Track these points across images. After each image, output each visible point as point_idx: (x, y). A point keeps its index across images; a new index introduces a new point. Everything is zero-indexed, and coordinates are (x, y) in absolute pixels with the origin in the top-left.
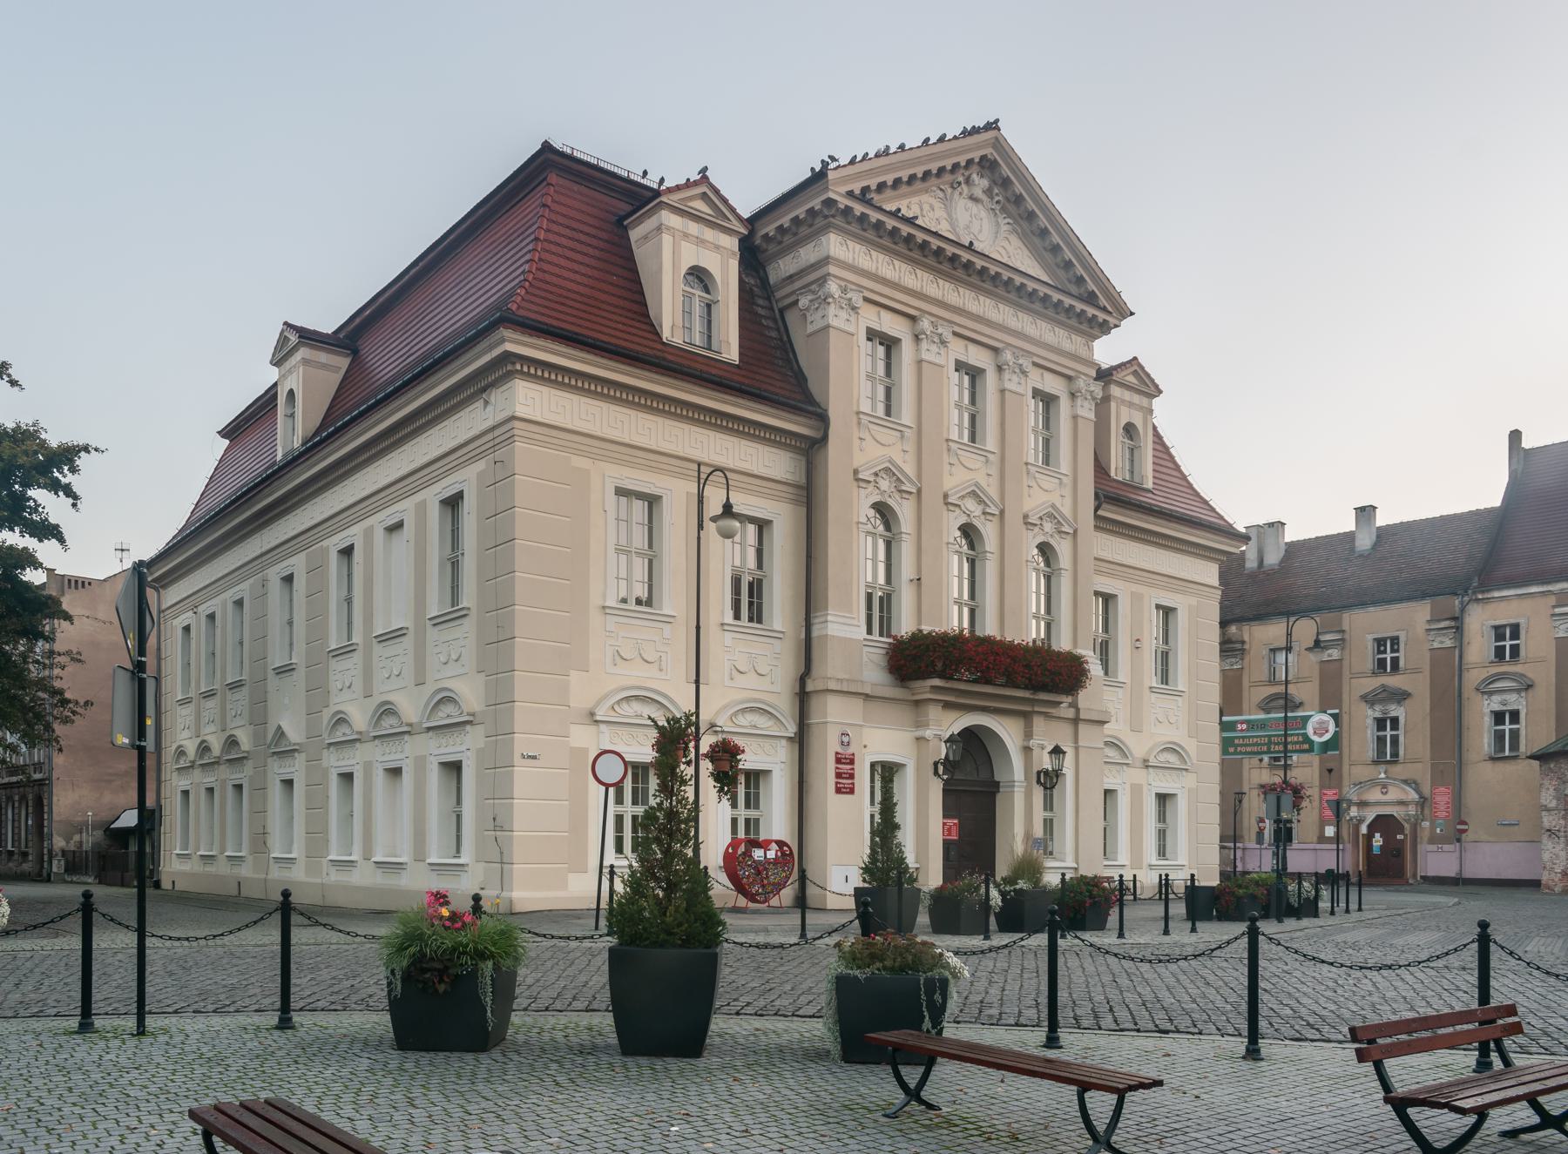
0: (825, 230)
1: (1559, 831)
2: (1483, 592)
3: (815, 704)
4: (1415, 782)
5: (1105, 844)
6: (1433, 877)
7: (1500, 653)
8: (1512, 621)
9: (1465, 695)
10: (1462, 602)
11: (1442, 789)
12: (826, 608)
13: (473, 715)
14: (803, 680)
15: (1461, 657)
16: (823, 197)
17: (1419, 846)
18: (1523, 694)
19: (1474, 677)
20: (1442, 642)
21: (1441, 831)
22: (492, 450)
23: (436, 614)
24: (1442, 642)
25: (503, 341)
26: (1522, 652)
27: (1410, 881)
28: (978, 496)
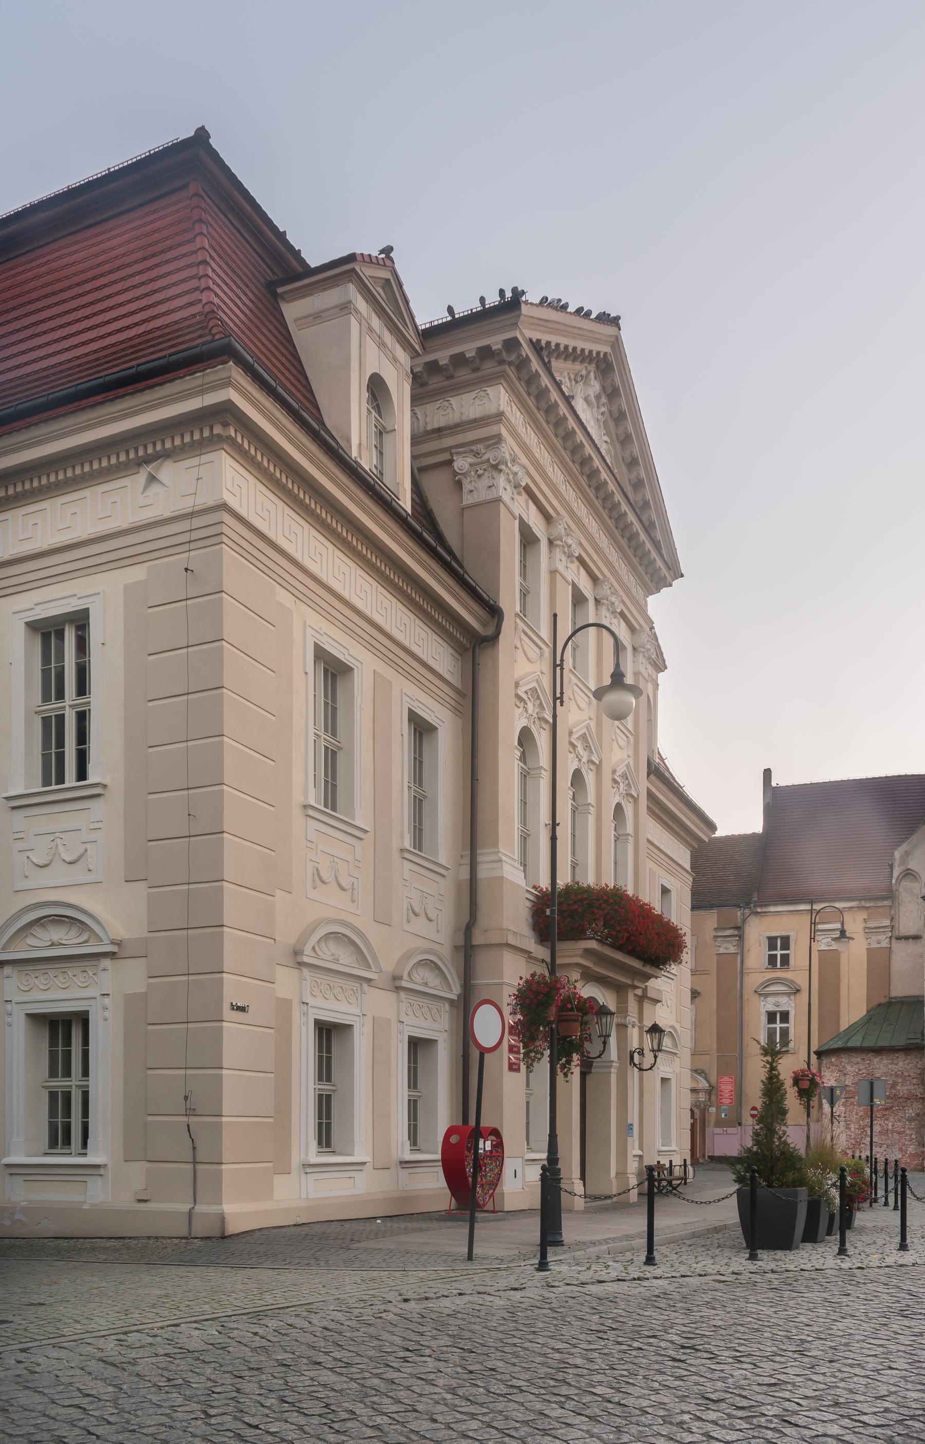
0: (491, 379)
1: (839, 1116)
2: (761, 906)
3: (482, 960)
4: (703, 1072)
5: (528, 1124)
6: (720, 1157)
7: (772, 960)
8: (784, 934)
9: (745, 996)
10: (743, 914)
11: (726, 1079)
12: (495, 844)
13: (119, 944)
14: (469, 929)
15: (742, 961)
16: (508, 335)
17: (707, 1129)
18: (792, 997)
19: (753, 981)
20: (727, 949)
21: (726, 1115)
22: (186, 547)
23: (21, 791)
24: (727, 949)
25: (227, 383)
26: (792, 961)
27: (701, 1161)
28: (587, 741)
